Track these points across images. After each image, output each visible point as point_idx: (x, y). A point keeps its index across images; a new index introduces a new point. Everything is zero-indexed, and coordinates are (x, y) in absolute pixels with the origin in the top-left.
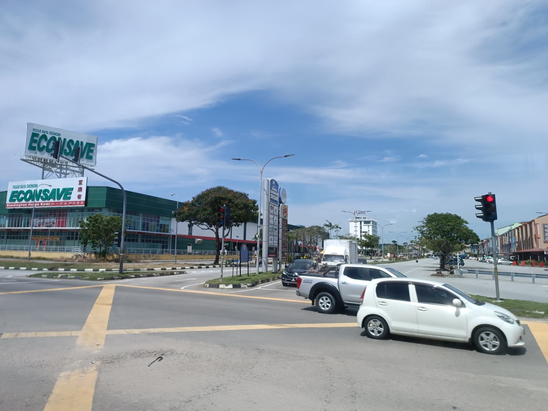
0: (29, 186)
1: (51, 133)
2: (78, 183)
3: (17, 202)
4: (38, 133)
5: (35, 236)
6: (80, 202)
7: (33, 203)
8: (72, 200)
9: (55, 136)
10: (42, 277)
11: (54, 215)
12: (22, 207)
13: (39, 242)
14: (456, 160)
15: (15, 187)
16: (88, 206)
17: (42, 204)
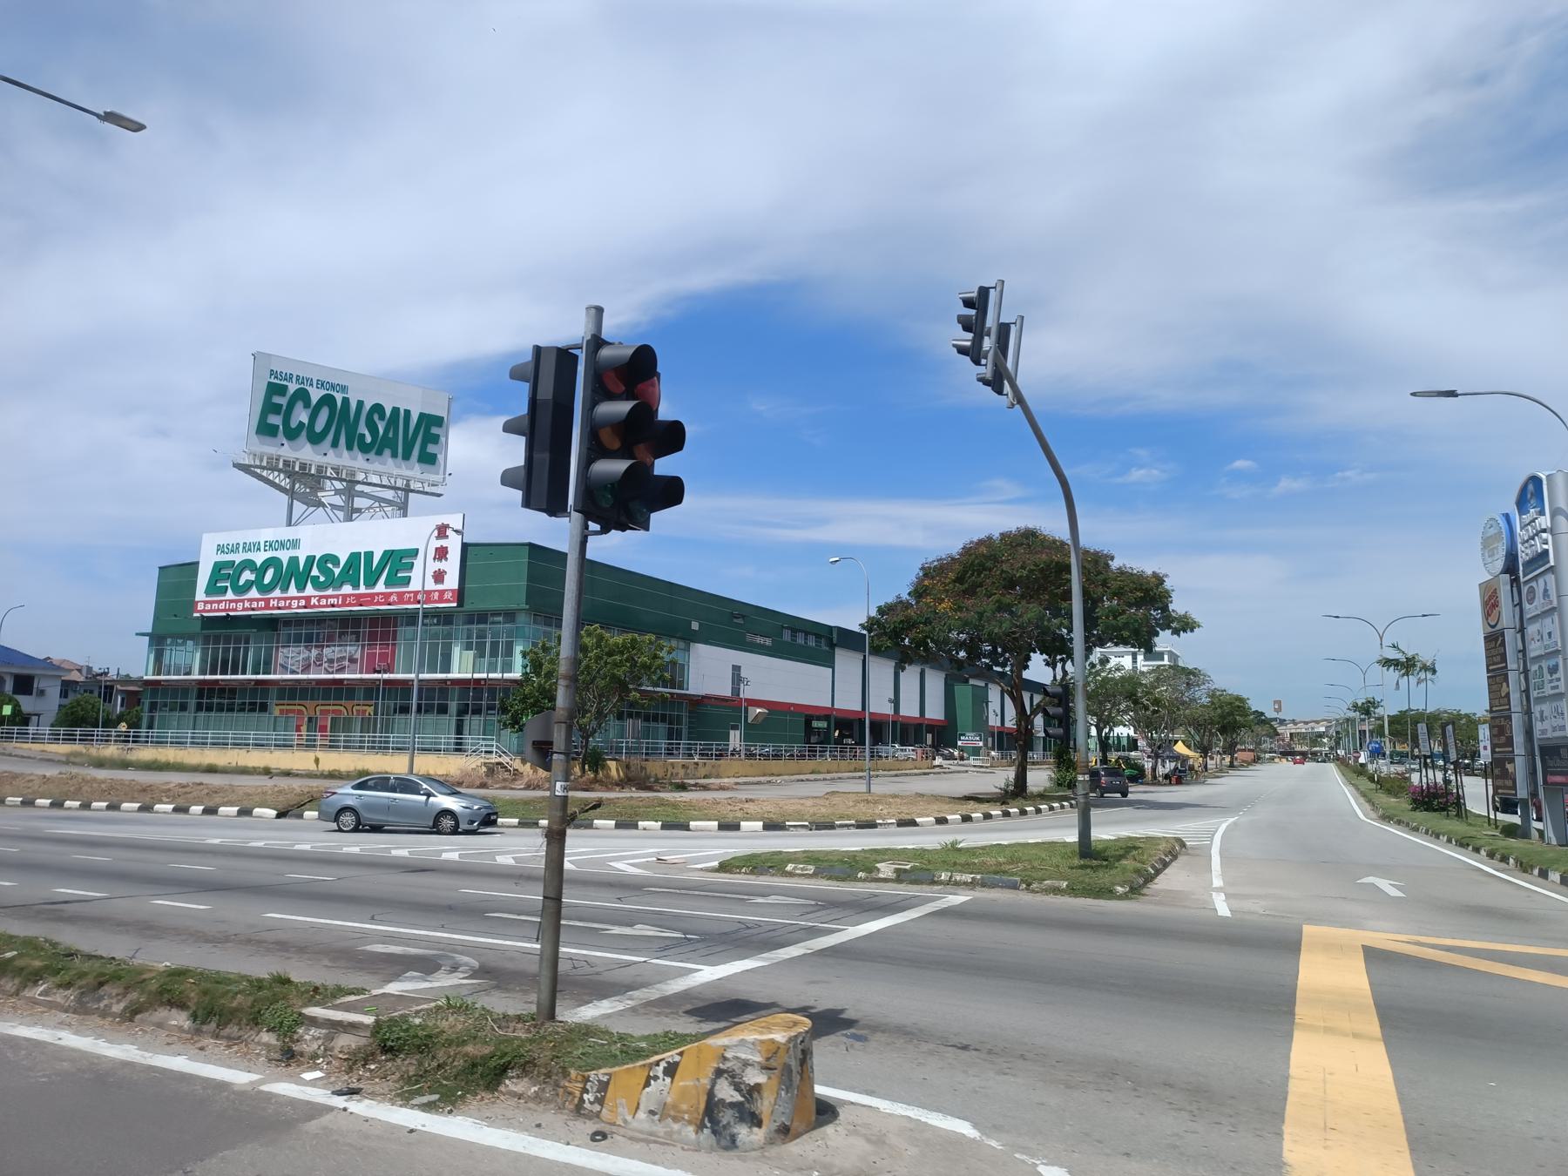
0: (271, 546)
1: (322, 385)
3: (230, 595)
4: (285, 383)
5: (282, 702)
6: (442, 592)
7: (285, 599)
8: (415, 585)
9: (332, 393)
10: (791, 874)
12: (247, 609)
13: (306, 719)
14: (1339, 474)
15: (226, 550)
16: (468, 607)
17: (314, 601)
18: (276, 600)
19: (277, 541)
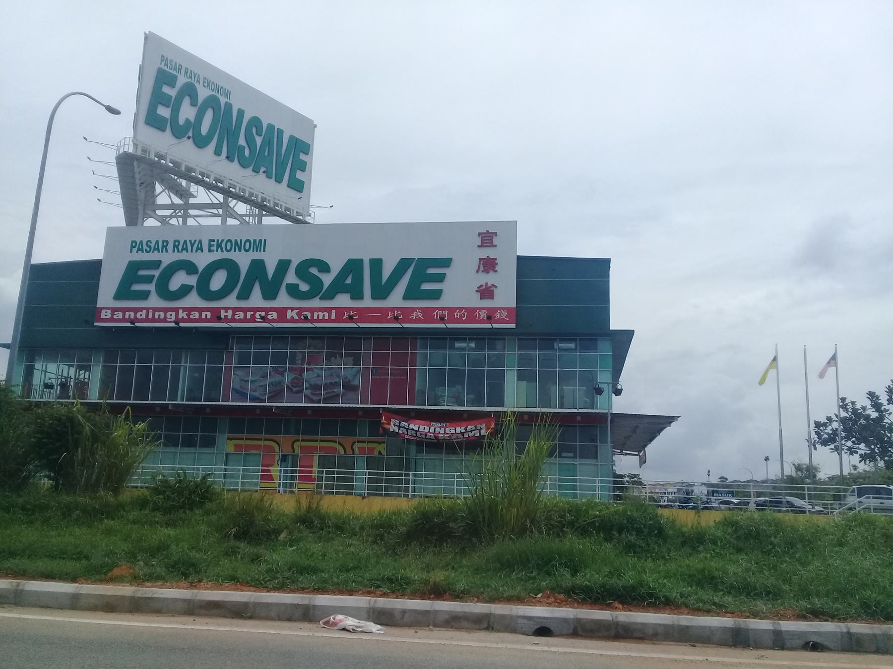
1: (208, 84)
2: (479, 241)
4: (174, 73)
7: (245, 310)
8: (445, 302)
9: (219, 96)
11: (351, 359)
17: (290, 314)
18: (230, 311)
19: (229, 241)
